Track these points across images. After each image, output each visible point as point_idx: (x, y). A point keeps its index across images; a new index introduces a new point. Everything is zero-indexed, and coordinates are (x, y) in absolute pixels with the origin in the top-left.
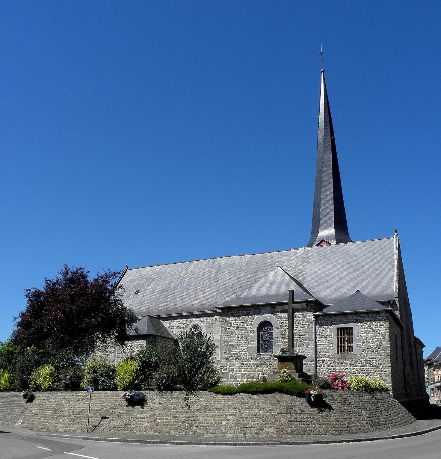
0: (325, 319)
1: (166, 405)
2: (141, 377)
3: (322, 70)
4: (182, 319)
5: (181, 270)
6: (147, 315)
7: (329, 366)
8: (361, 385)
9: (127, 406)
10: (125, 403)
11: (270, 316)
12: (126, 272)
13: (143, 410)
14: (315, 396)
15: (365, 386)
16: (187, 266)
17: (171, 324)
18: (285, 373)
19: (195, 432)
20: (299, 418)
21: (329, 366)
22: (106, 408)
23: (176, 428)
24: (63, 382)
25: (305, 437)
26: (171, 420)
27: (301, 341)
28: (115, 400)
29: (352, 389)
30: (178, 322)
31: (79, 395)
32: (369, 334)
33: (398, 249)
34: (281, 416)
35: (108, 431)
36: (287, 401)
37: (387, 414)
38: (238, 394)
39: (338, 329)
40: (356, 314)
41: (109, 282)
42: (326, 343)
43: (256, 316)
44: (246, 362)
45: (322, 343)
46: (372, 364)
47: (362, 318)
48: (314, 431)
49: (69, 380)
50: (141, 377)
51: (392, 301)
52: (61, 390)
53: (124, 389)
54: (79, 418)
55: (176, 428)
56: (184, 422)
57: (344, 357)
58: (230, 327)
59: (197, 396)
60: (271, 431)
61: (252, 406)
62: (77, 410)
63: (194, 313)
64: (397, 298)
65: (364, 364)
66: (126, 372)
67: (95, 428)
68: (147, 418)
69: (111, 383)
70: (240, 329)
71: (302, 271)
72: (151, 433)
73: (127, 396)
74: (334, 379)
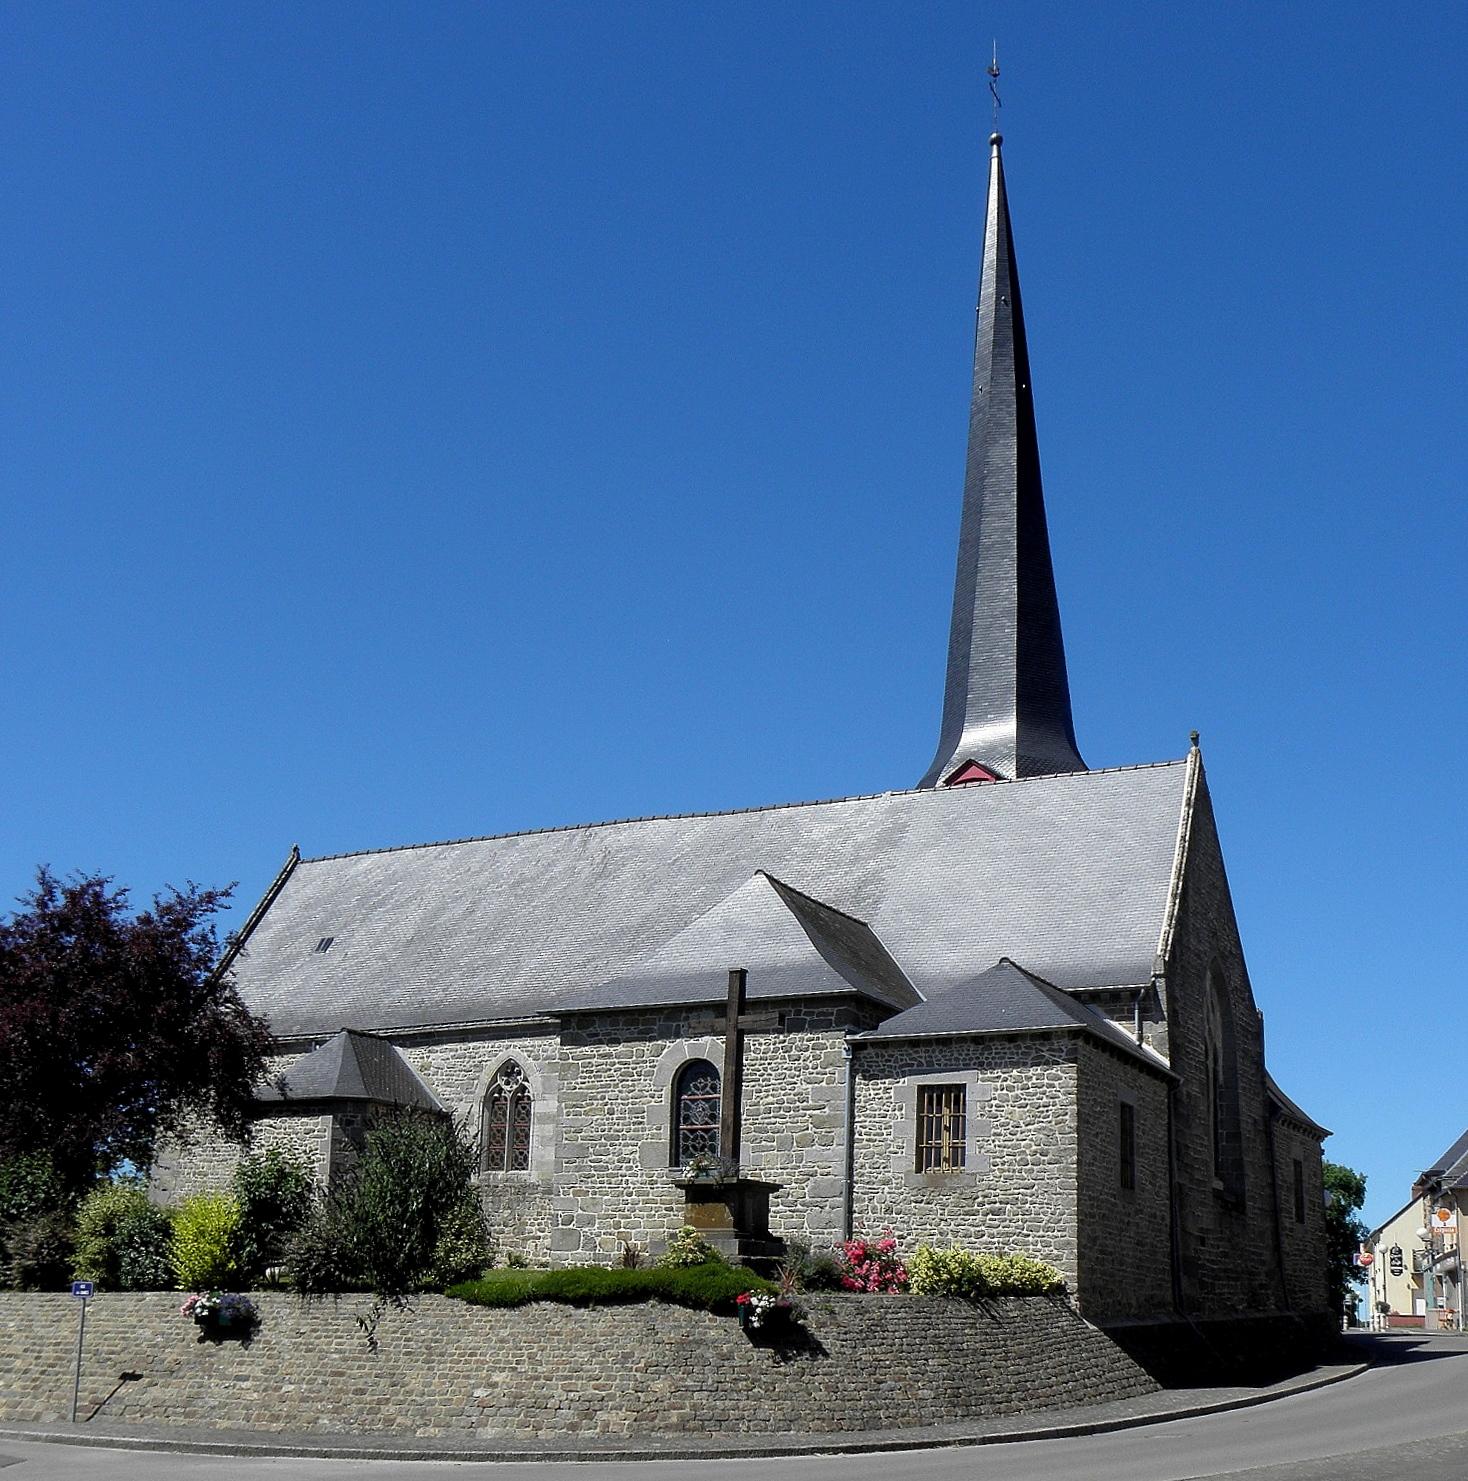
0: (883, 1056)
1: (315, 1338)
2: (248, 1249)
3: (994, 135)
4: (463, 1041)
5: (475, 867)
6: (343, 1029)
7: (889, 1210)
8: (945, 1276)
9: (201, 1340)
10: (196, 1331)
11: (713, 1043)
12: (292, 870)
13: (247, 1352)
14: (763, 1312)
15: (958, 1281)
16: (499, 853)
17: (428, 1057)
18: (689, 1240)
19: (389, 1421)
20: (710, 1382)
21: (889, 1210)
22: (137, 1345)
23: (336, 1411)
24: (14, 1263)
25: (720, 1439)
26: (325, 1383)
27: (807, 1129)
28: (167, 1322)
29: (915, 1290)
30: (453, 1054)
31: (59, 1306)
32: (1016, 1108)
33: (1192, 804)
34: (655, 1372)
35: (134, 1419)
36: (681, 1327)
37: (1022, 1369)
38: (535, 1305)
39: (922, 1089)
40: (978, 1039)
41: (191, 925)
42: (885, 1136)
43: (668, 1044)
44: (634, 1197)
45: (872, 1137)
46: (1019, 1205)
47: (996, 1053)
48: (750, 1421)
49: (34, 1255)
50: (248, 1249)
51: (1143, 991)
52: (11, 1288)
53: (195, 1287)
54: (55, 1378)
55: (336, 1411)
56: (362, 1392)
57: (936, 1183)
58: (587, 1080)
59: (409, 1309)
60: (616, 1419)
61: (571, 1342)
62: (49, 1353)
63: (503, 1023)
64: (1163, 980)
65: (998, 1205)
66: (202, 1233)
67: (98, 1409)
68: (256, 1379)
69: (156, 1268)
70: (616, 1086)
71: (874, 878)
72: (262, 1426)
73: (199, 1310)
74: (857, 1257)
